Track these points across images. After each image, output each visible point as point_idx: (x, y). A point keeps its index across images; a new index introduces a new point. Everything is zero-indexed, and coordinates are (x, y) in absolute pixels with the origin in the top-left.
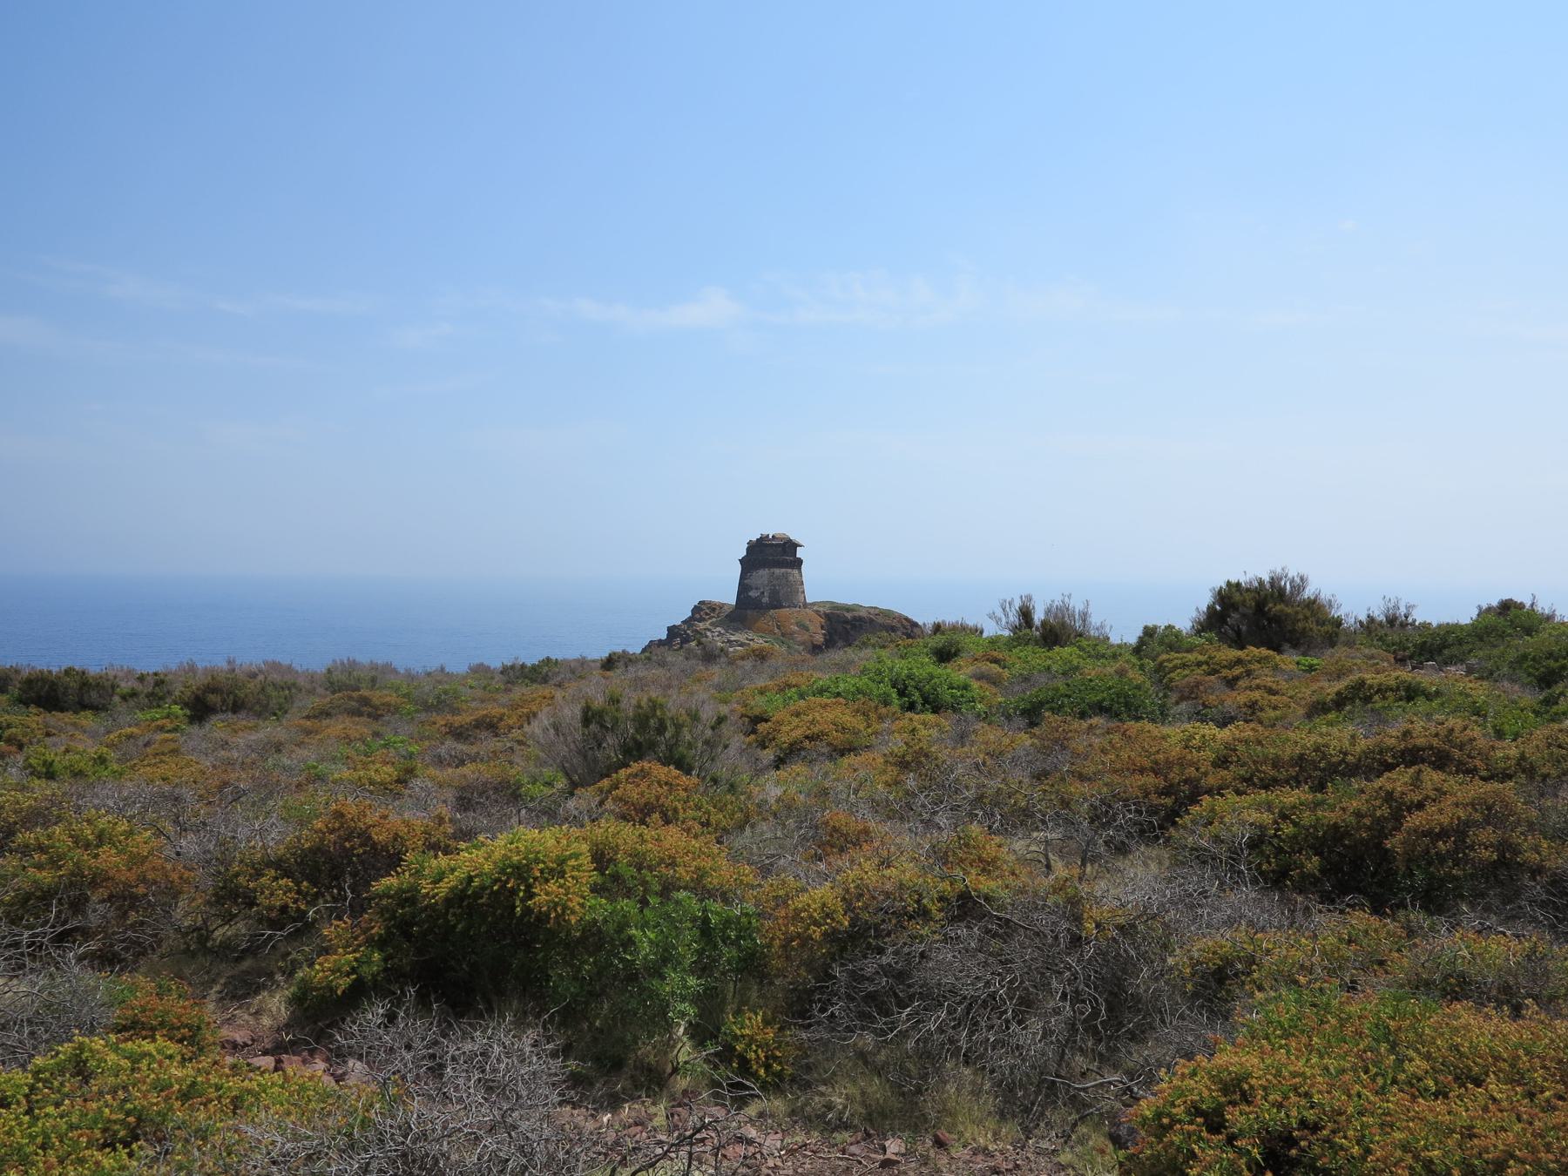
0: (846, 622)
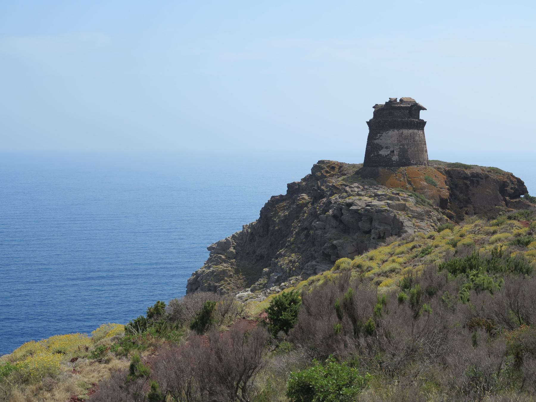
0: (466, 178)
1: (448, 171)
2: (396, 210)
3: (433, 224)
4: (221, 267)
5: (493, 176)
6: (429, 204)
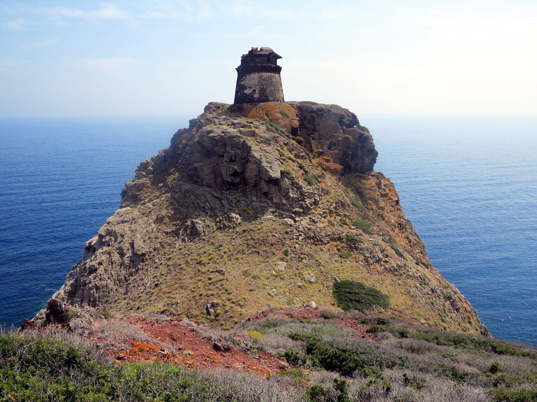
0: (313, 111)
1: (299, 107)
2: (247, 136)
3: (279, 148)
4: (141, 181)
5: (334, 111)
6: (281, 131)
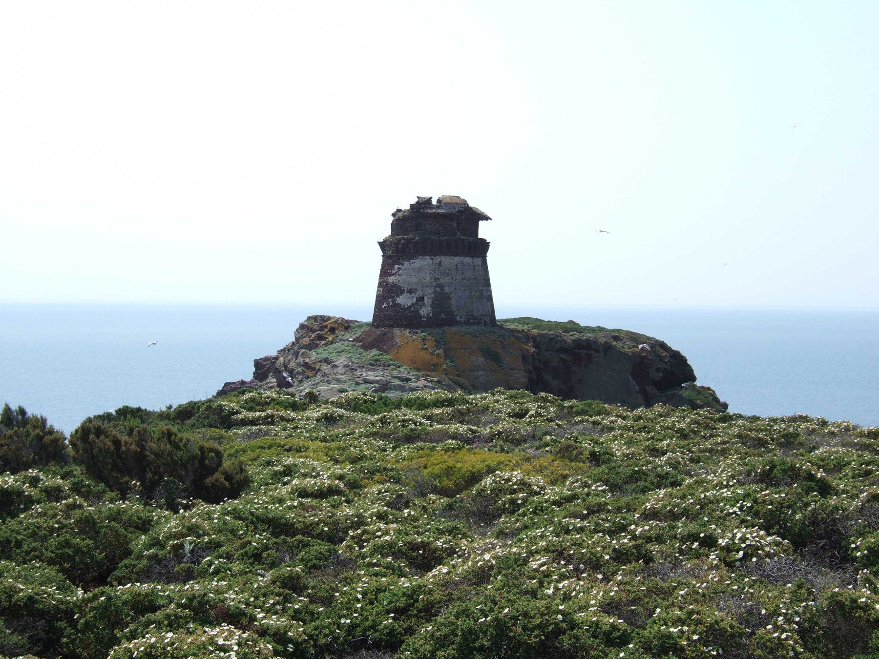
0: (565, 349)
